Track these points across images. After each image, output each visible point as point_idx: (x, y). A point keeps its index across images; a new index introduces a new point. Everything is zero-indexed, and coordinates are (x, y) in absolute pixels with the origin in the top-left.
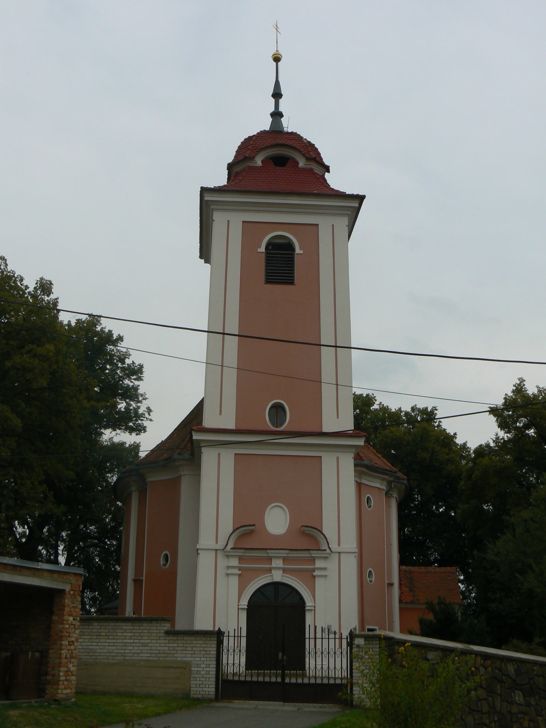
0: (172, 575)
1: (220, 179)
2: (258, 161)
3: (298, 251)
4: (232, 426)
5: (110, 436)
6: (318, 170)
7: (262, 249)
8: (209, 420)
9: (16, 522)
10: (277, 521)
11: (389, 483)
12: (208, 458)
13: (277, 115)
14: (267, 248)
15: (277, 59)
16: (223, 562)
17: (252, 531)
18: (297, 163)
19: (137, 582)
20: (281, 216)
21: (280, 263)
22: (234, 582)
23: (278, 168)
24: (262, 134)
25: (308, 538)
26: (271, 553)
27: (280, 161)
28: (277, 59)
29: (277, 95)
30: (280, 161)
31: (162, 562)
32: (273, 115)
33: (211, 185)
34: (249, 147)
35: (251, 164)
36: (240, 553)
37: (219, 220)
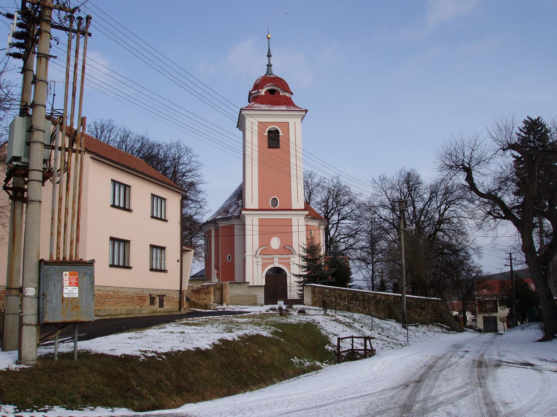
2: (263, 92)
3: (281, 134)
5: (292, 359)
6: (288, 95)
7: (266, 134)
10: (275, 243)
13: (269, 66)
18: (279, 93)
20: (274, 117)
21: (274, 139)
22: (260, 267)
25: (287, 249)
26: (274, 256)
29: (269, 56)
31: (228, 258)
32: (268, 66)
35: (260, 94)
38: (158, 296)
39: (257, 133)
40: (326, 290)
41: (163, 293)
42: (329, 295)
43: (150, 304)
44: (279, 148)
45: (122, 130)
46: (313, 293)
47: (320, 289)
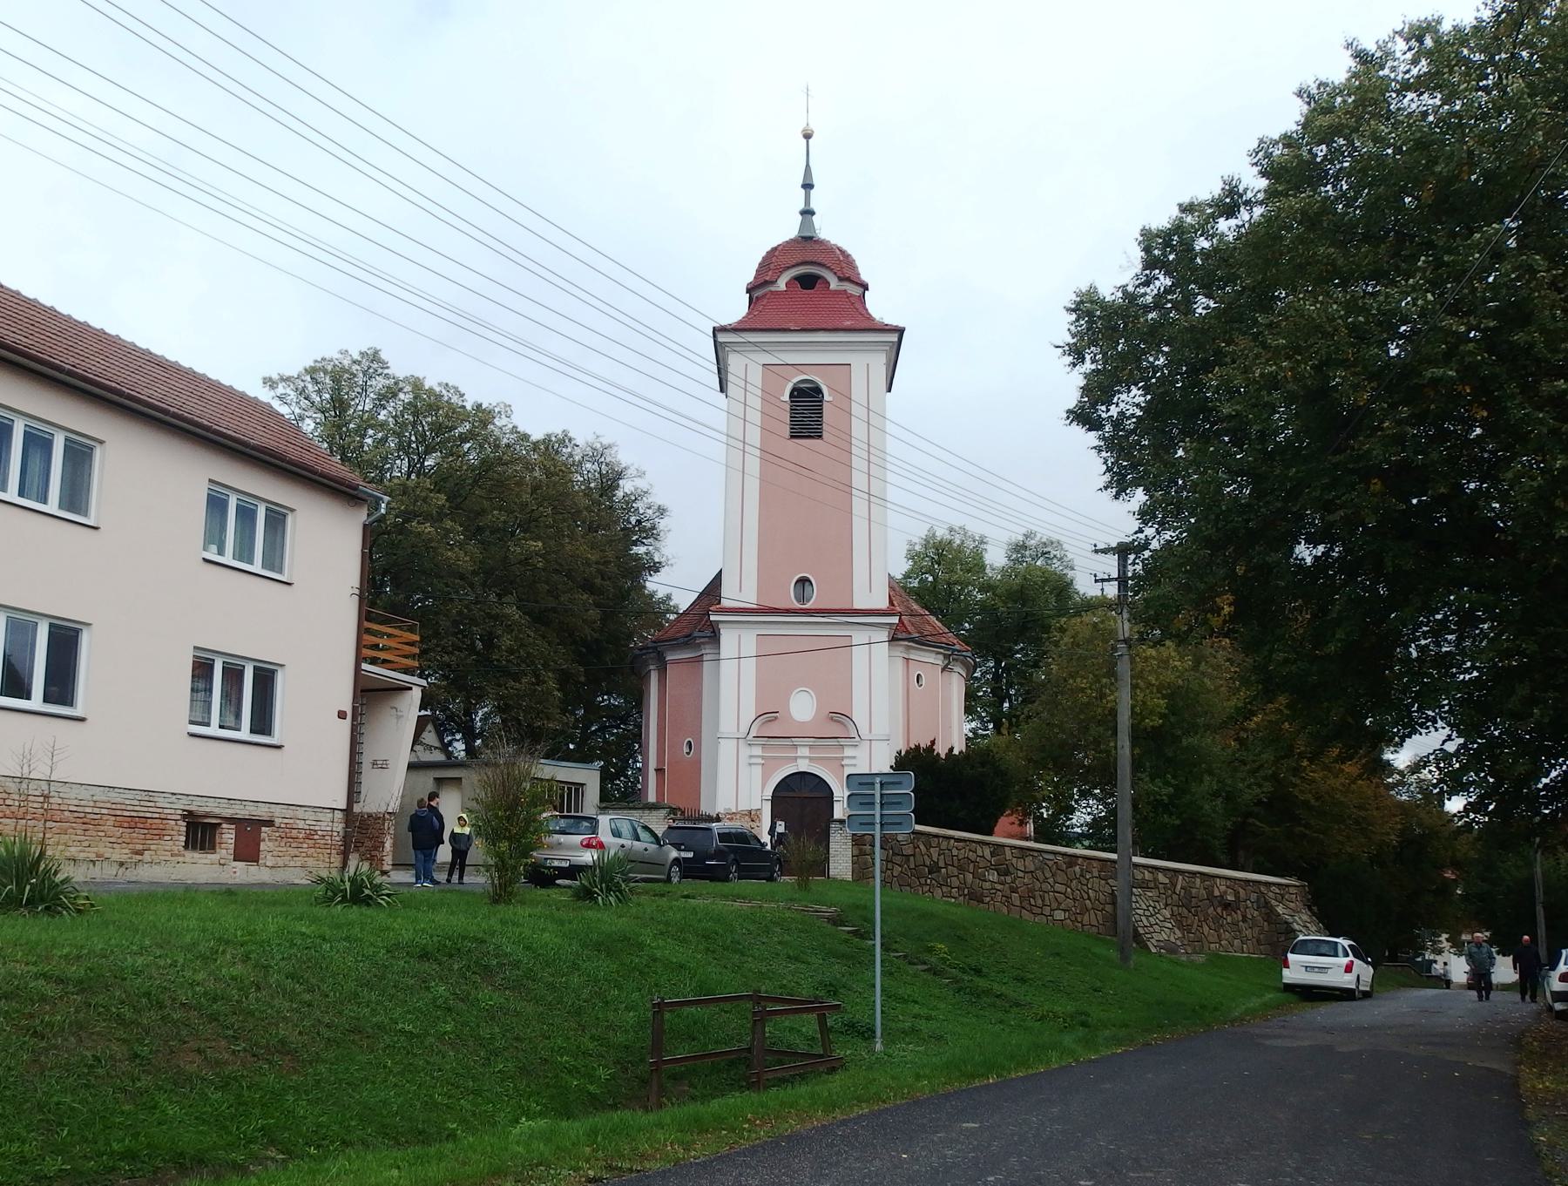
0: (697, 764)
1: (736, 308)
2: (781, 285)
3: (826, 397)
6: (854, 290)
7: (786, 397)
8: (731, 595)
9: (1445, 936)
10: (803, 708)
11: (946, 657)
12: (729, 639)
13: (807, 213)
14: (791, 395)
15: (808, 136)
16: (745, 751)
19: (659, 771)
20: (807, 356)
21: (806, 410)
22: (758, 771)
23: (807, 287)
28: (808, 136)
29: (808, 186)
30: (808, 282)
31: (686, 750)
33: (724, 322)
37: (735, 362)
38: (230, 820)
39: (759, 393)
41: (262, 812)
42: (908, 850)
43: (186, 847)
44: (820, 437)
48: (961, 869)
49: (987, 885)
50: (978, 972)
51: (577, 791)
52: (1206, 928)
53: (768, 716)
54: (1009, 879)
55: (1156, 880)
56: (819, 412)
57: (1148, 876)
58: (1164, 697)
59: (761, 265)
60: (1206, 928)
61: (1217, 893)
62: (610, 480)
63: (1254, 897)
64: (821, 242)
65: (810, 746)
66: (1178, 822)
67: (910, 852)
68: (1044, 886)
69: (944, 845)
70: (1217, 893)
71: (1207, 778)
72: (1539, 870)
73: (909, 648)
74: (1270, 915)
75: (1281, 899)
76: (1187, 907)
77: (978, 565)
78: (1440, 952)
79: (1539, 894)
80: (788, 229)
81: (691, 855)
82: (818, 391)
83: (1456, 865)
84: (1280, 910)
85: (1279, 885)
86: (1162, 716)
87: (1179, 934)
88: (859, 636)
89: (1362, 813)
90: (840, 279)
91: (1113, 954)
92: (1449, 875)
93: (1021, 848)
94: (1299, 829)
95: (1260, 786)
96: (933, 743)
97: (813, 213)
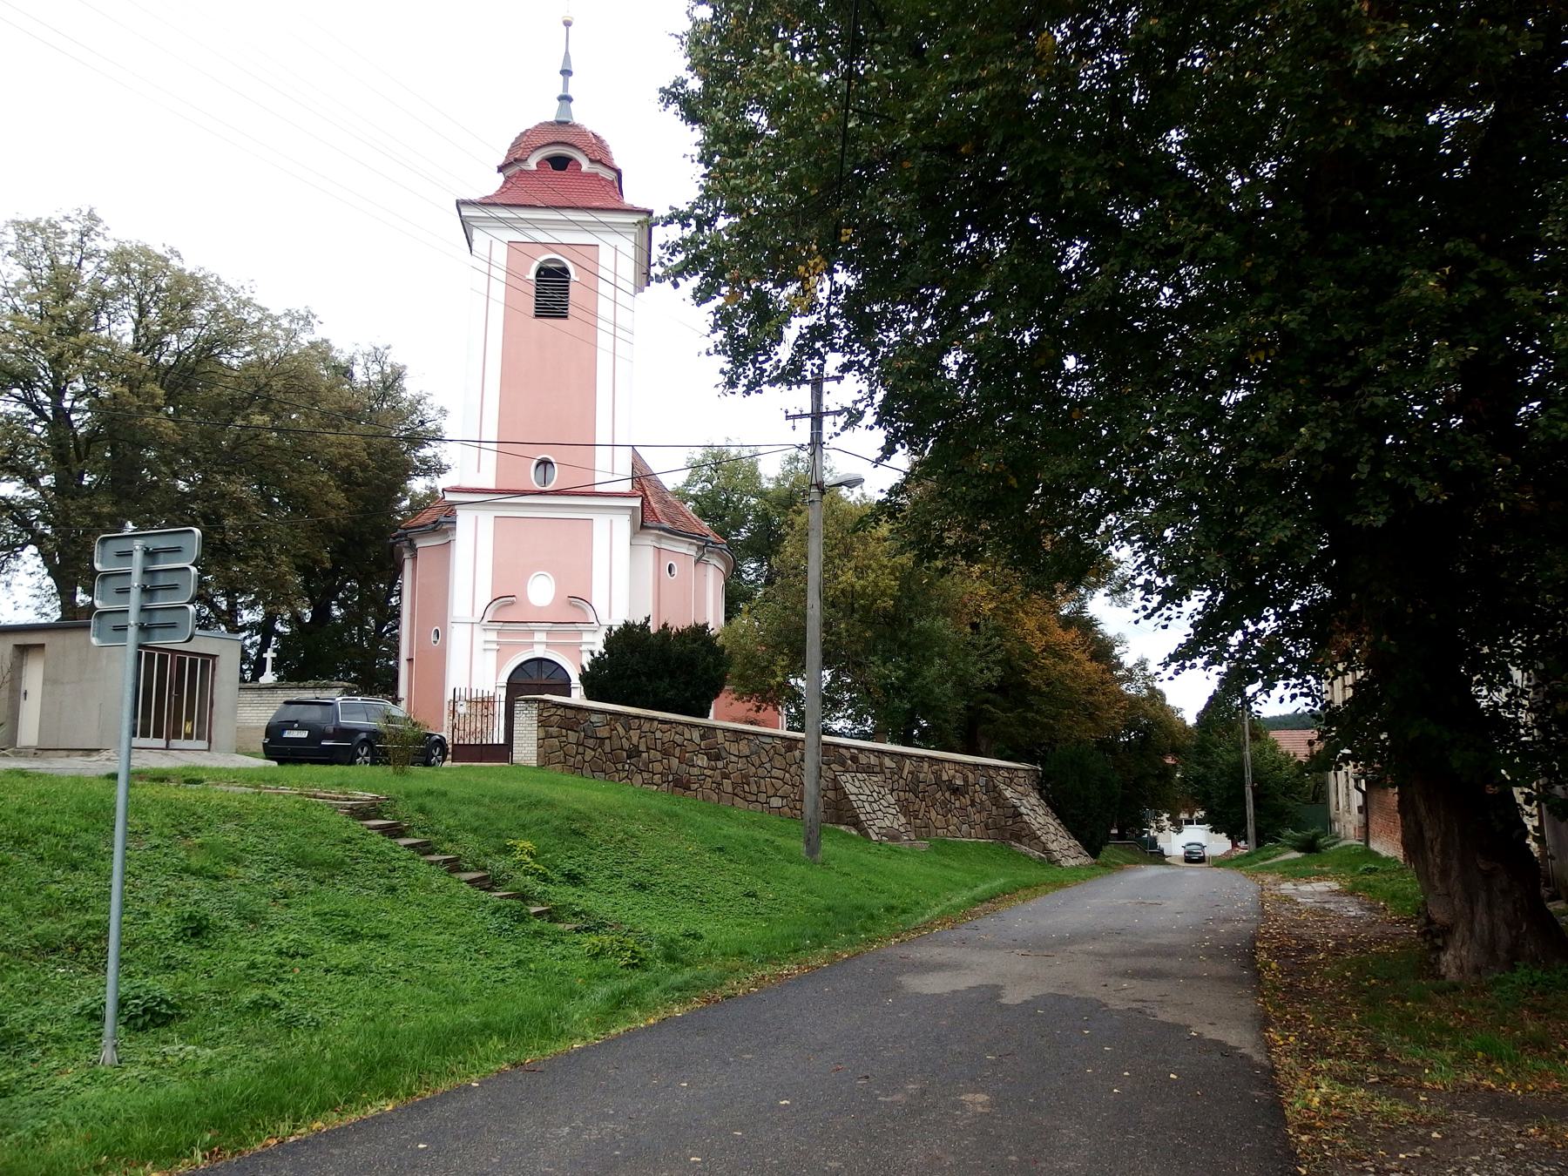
2: (532, 164)
4: (492, 486)
7: (532, 275)
9: (1167, 815)
10: (541, 592)
11: (699, 548)
13: (565, 99)
14: (538, 275)
15: (567, 24)
16: (480, 636)
17: (513, 603)
20: (558, 234)
21: (552, 290)
22: (492, 657)
24: (543, 127)
27: (560, 163)
28: (567, 24)
29: (566, 73)
30: (560, 163)
32: (561, 98)
34: (524, 144)
36: (498, 626)
40: (594, 718)
42: (603, 732)
45: (85, 212)
46: (543, 723)
47: (570, 714)
48: (666, 753)
49: (695, 771)
50: (573, 879)
51: (205, 664)
52: (933, 813)
53: (503, 600)
54: (720, 764)
55: (881, 764)
56: (565, 291)
57: (873, 760)
58: (896, 579)
59: (514, 145)
60: (933, 813)
61: (945, 777)
62: (391, 383)
63: (982, 781)
64: (574, 126)
65: (548, 632)
66: (908, 706)
67: (606, 735)
68: (760, 771)
69: (646, 727)
70: (945, 777)
71: (937, 661)
72: (1247, 753)
73: (660, 537)
74: (998, 799)
75: (1010, 782)
76: (914, 794)
77: (753, 475)
78: (1161, 830)
79: (1248, 776)
80: (549, 112)
81: (304, 734)
82: (565, 271)
83: (1175, 751)
84: (1008, 793)
85: (1008, 768)
86: (893, 597)
87: (903, 820)
88: (601, 523)
89: (1091, 699)
90: (591, 161)
91: (798, 846)
92: (1169, 761)
93: (735, 731)
94: (1030, 715)
95: (991, 670)
96: (648, 619)
97: (570, 99)
